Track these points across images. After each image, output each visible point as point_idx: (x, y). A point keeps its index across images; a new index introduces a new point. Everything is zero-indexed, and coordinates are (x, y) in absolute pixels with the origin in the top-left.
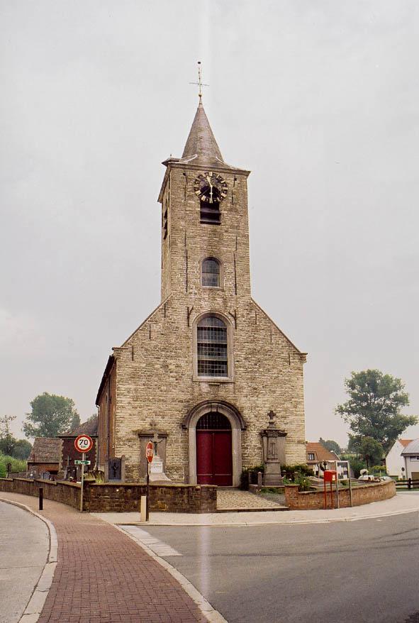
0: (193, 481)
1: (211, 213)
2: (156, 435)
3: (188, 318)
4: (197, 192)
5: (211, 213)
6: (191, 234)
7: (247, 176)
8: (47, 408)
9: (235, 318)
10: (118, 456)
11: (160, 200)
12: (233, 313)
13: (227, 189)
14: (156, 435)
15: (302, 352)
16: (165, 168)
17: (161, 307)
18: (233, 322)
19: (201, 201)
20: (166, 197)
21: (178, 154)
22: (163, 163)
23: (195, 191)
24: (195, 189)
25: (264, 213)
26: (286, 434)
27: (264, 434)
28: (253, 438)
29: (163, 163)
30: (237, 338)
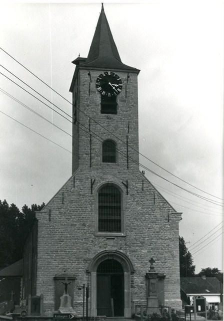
0: (94, 313)
1: (109, 105)
2: (66, 279)
3: (92, 187)
4: (98, 89)
5: (109, 105)
6: (49, 294)
7: (138, 74)
8: (5, 202)
9: (127, 187)
10: (38, 294)
11: (71, 90)
12: (126, 183)
13: (122, 85)
14: (66, 279)
15: (178, 212)
16: (75, 66)
17: (71, 180)
18: (125, 190)
19: (102, 96)
20: (75, 88)
21: (85, 55)
22: (72, 62)
23: (97, 87)
24: (97, 86)
25: (153, 96)
26: (165, 276)
27: (148, 277)
28: (139, 280)
29: (72, 62)
30: (130, 207)
